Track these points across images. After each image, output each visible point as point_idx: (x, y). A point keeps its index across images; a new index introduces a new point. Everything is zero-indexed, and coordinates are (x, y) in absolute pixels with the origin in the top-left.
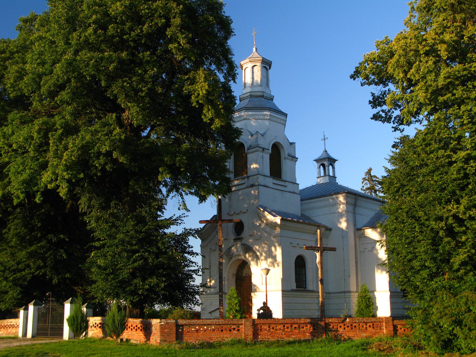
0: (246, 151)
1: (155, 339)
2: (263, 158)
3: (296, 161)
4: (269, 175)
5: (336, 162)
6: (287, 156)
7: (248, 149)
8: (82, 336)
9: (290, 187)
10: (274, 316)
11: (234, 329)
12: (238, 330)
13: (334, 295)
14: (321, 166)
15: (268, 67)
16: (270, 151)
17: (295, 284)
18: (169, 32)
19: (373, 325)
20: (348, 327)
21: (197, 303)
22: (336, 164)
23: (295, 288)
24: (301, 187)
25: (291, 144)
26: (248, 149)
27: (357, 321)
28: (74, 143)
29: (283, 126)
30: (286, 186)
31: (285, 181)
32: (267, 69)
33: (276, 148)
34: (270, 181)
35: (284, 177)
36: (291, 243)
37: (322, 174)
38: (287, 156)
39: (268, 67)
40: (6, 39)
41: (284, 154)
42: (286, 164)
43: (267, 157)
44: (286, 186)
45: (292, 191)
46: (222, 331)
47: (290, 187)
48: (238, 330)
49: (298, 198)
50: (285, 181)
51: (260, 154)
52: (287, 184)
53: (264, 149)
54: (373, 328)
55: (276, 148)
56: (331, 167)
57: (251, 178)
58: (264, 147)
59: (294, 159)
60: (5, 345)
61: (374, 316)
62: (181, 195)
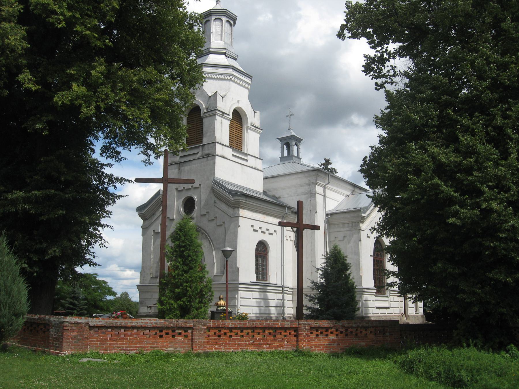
4: (228, 145)
6: (249, 125)
13: (366, 290)
16: (231, 117)
21: (52, 18)
22: (301, 146)
23: (254, 280)
30: (247, 160)
32: (231, 25)
34: (229, 152)
36: (252, 226)
37: (285, 154)
38: (249, 125)
44: (247, 160)
45: (254, 167)
46: (161, 336)
50: (246, 155)
52: (249, 158)
53: (223, 113)
56: (295, 147)
57: (206, 146)
58: (224, 111)
61: (138, 303)
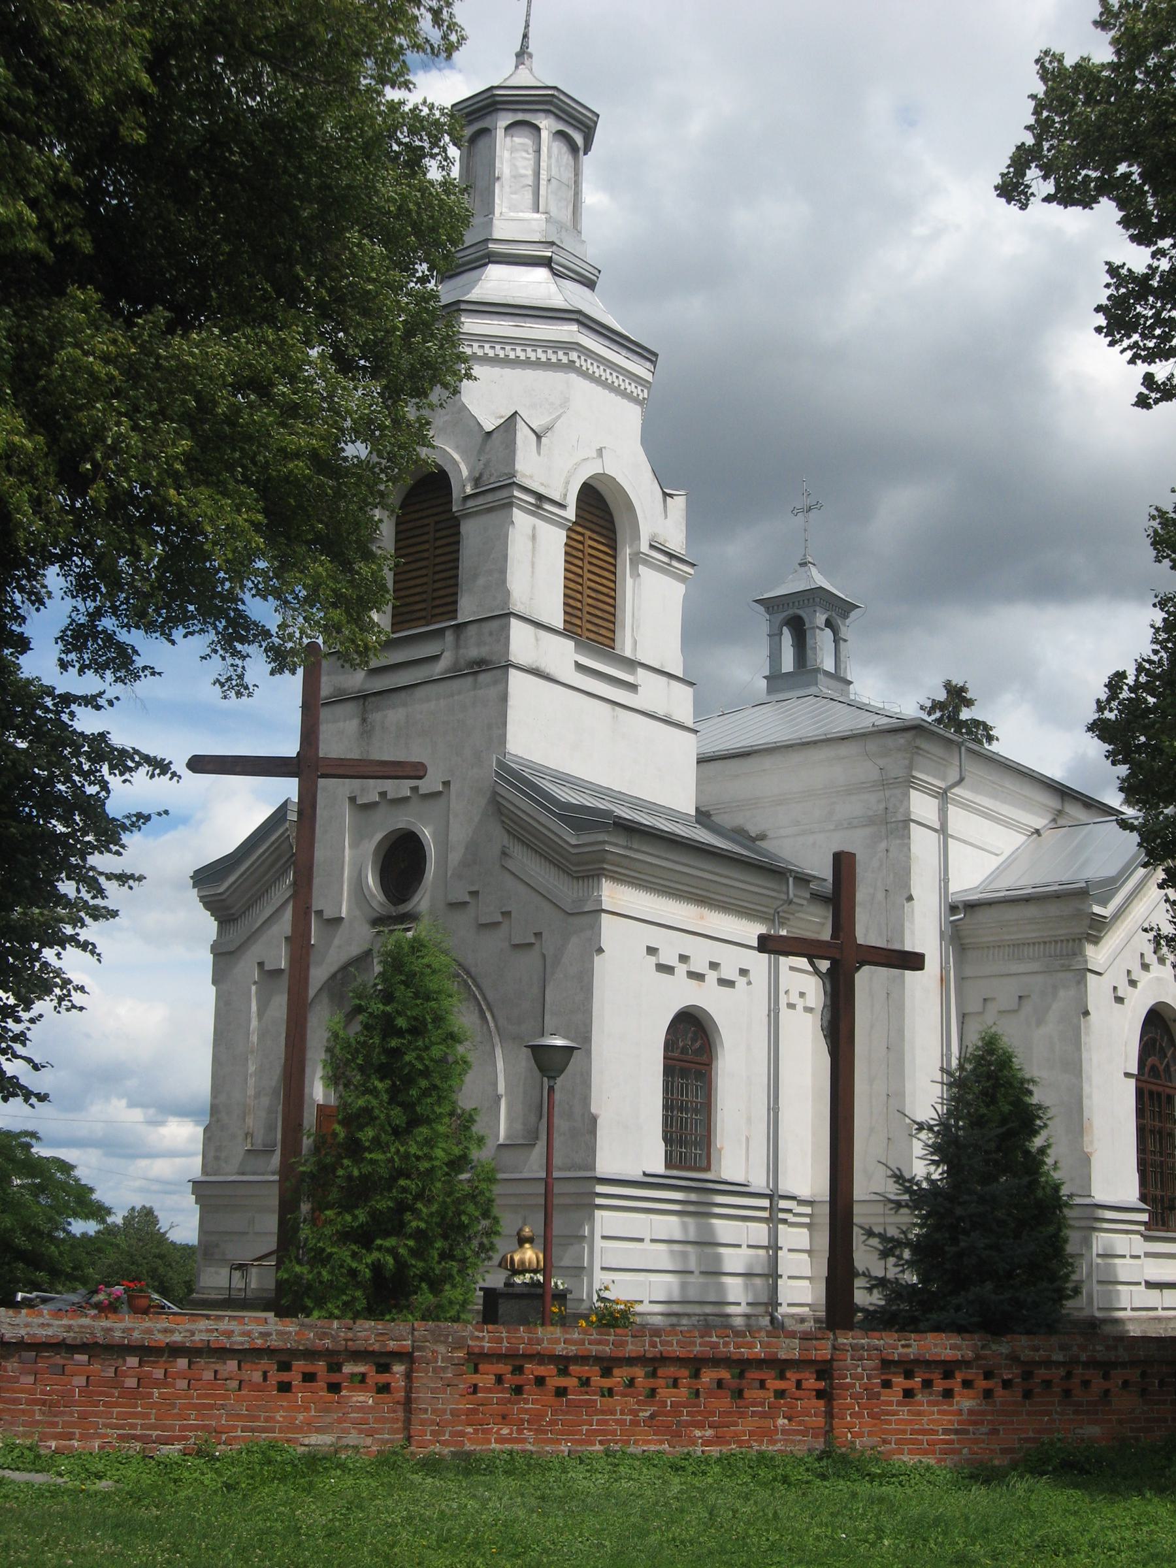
2: (534, 537)
5: (854, 614)
6: (644, 548)
13: (1109, 1215)
14: (785, 630)
15: (579, 139)
16: (571, 514)
17: (661, 1146)
19: (1144, 1375)
20: (1007, 1384)
27: (1058, 1357)
30: (633, 687)
32: (574, 149)
34: (561, 655)
36: (652, 951)
37: (788, 664)
39: (579, 139)
44: (633, 687)
45: (661, 713)
46: (284, 1387)
50: (632, 664)
52: (641, 677)
53: (540, 497)
54: (1144, 1392)
57: (472, 630)
58: (542, 490)
62: (73, 939)
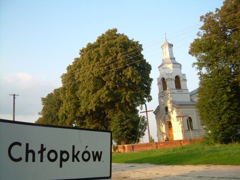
0: (166, 81)
1: (127, 151)
3: (186, 81)
7: (166, 80)
8: (117, 151)
9: (185, 91)
10: (155, 141)
11: (151, 146)
12: (152, 146)
16: (175, 79)
18: (118, 58)
24: (190, 91)
25: (184, 75)
26: (166, 80)
28: (95, 96)
29: (180, 69)
31: (182, 90)
33: (177, 78)
34: (176, 91)
35: (182, 88)
40: (76, 58)
41: (181, 79)
42: (182, 83)
43: (173, 82)
47: (185, 91)
48: (152, 146)
49: (189, 95)
50: (182, 90)
51: (171, 81)
52: (183, 91)
53: (171, 79)
55: (177, 78)
59: (185, 80)
60: (213, 168)
